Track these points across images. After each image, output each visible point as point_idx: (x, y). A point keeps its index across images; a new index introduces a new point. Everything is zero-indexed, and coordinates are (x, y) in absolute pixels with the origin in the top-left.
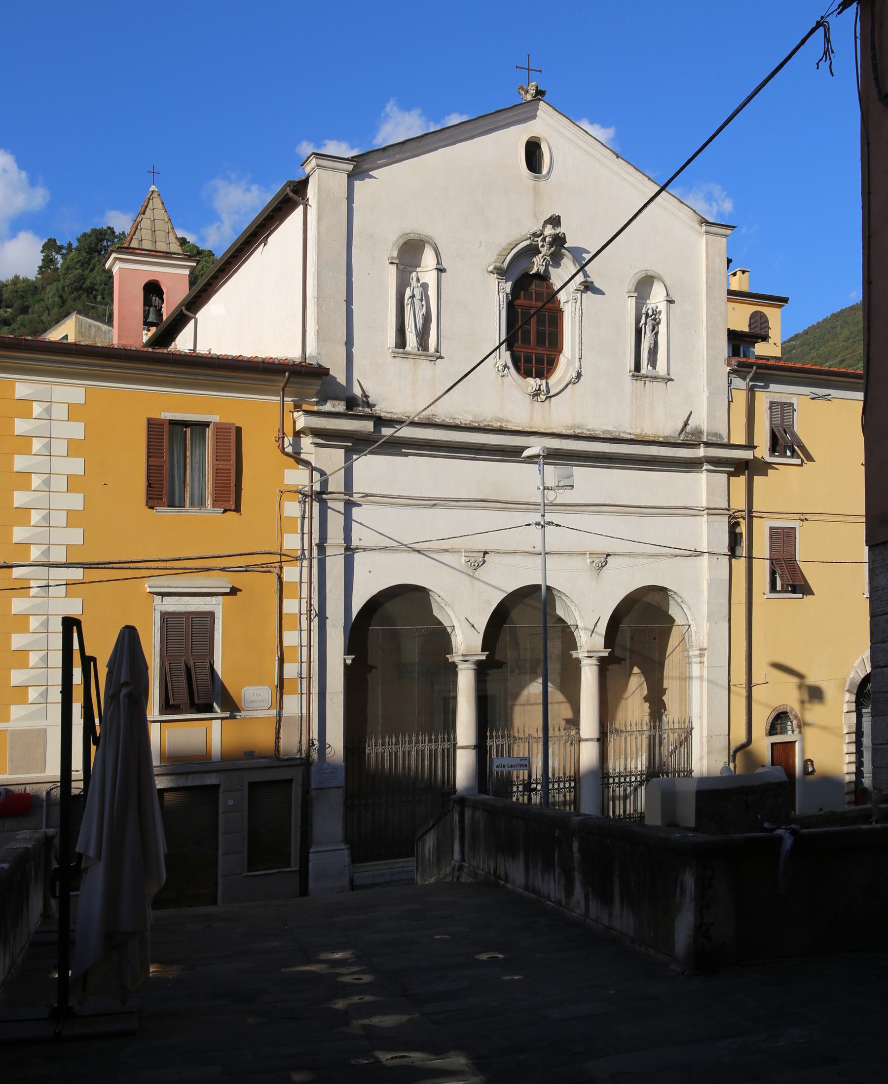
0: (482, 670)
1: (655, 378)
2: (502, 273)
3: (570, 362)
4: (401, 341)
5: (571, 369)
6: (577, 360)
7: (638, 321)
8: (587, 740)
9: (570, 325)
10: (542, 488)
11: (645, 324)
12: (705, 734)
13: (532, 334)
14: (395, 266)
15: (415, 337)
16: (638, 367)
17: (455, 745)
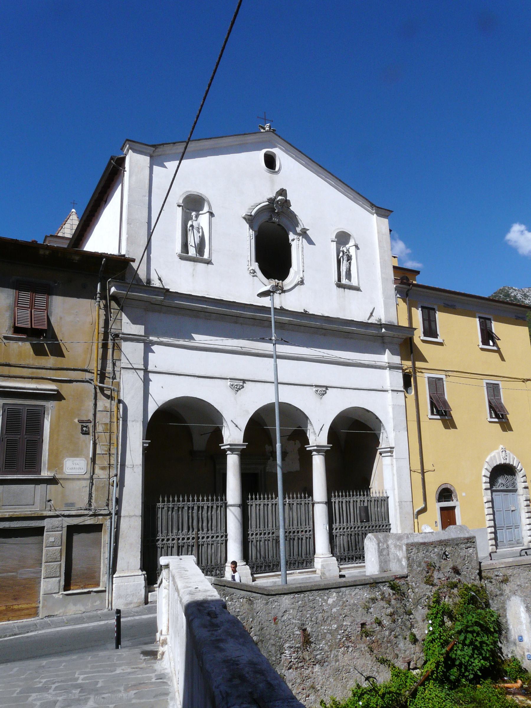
0: (245, 456)
1: (351, 288)
2: (250, 220)
3: (296, 273)
4: (185, 246)
5: (298, 276)
6: (301, 272)
7: (338, 255)
8: (318, 503)
9: (296, 255)
10: (276, 382)
11: (343, 258)
12: (397, 500)
13: (273, 253)
14: (181, 208)
15: (195, 252)
16: (339, 279)
17: (226, 504)
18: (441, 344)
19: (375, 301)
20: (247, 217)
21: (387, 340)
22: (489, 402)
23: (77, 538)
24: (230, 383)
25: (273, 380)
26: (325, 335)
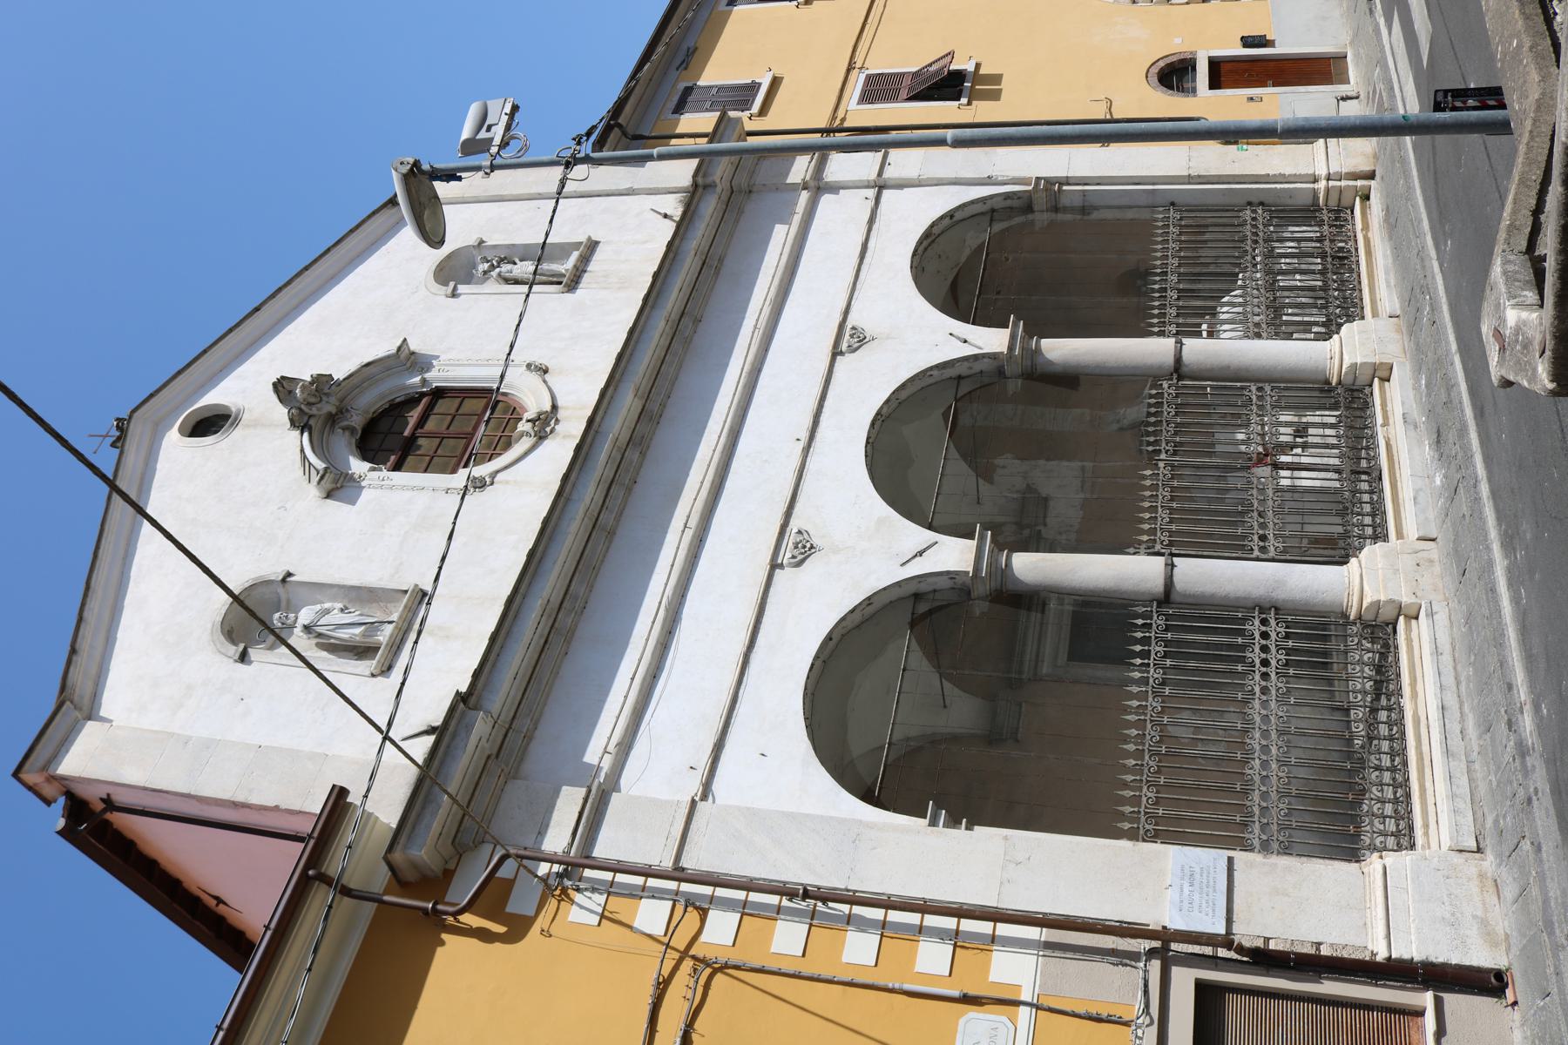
18: (776, 82)
19: (631, 219)
20: (327, 483)
21: (742, 180)
22: (910, 99)
23: (23, 776)
24: (795, 526)
25: (871, 193)
26: (697, 321)
